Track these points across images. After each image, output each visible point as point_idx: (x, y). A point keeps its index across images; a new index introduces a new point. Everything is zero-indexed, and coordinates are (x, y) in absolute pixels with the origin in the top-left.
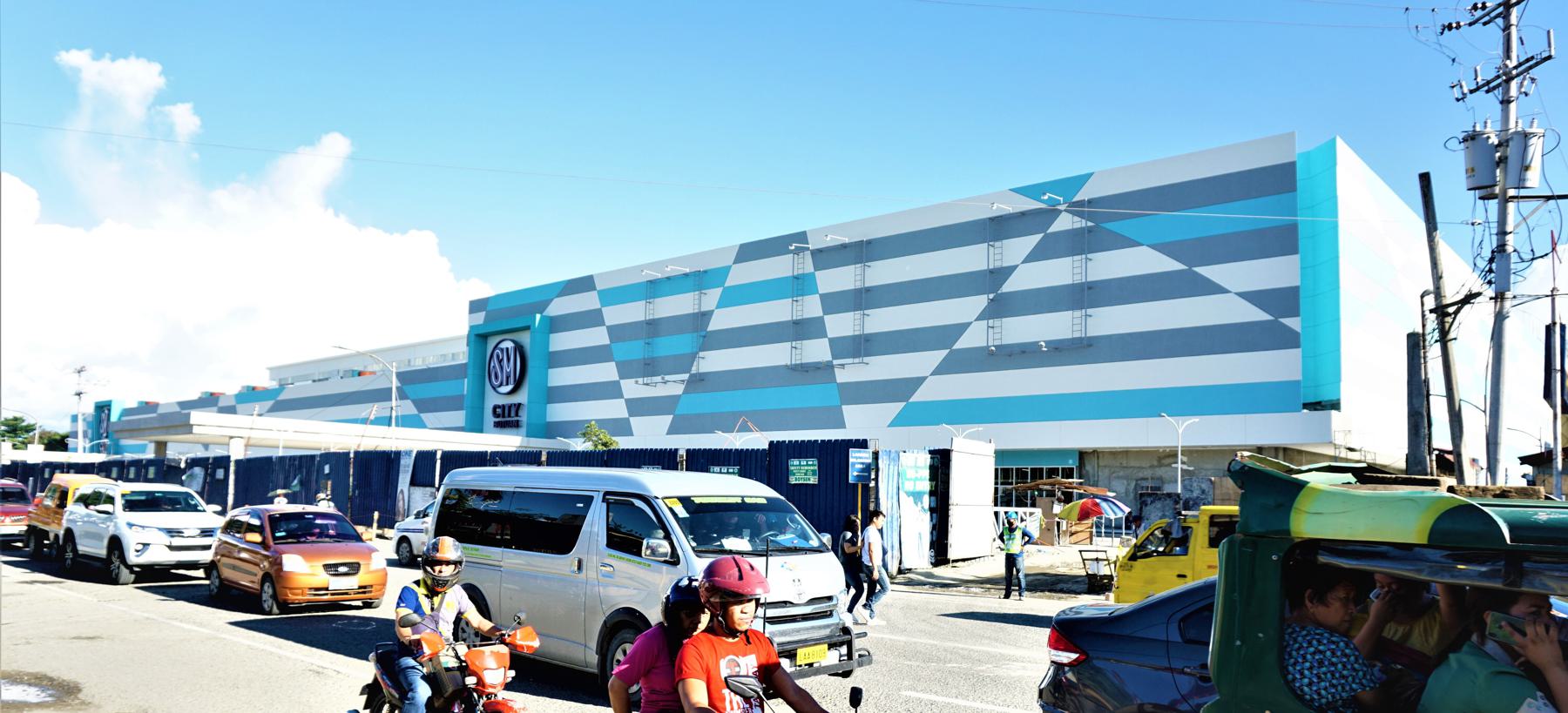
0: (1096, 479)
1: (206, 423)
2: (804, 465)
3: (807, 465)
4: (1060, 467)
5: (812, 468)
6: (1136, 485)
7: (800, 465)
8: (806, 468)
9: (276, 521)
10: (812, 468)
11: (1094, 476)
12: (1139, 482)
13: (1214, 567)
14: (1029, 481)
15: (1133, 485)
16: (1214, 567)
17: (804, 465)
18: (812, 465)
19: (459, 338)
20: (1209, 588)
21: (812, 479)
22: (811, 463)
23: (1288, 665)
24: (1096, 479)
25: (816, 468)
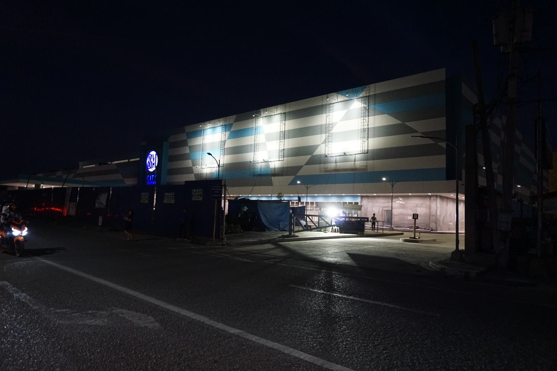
0: (367, 207)
1: (386, 202)
2: (197, 192)
3: (199, 192)
4: (315, 202)
5: (200, 193)
6: (382, 209)
7: (196, 192)
8: (198, 193)
9: (348, 300)
10: (200, 193)
11: (366, 206)
12: (383, 208)
13: (463, 185)
14: (295, 205)
15: (381, 209)
16: (463, 185)
17: (197, 192)
18: (201, 192)
19: (394, 202)
20: (446, 143)
21: (200, 198)
22: (200, 191)
23: (448, 224)
24: (367, 207)
25: (202, 193)
